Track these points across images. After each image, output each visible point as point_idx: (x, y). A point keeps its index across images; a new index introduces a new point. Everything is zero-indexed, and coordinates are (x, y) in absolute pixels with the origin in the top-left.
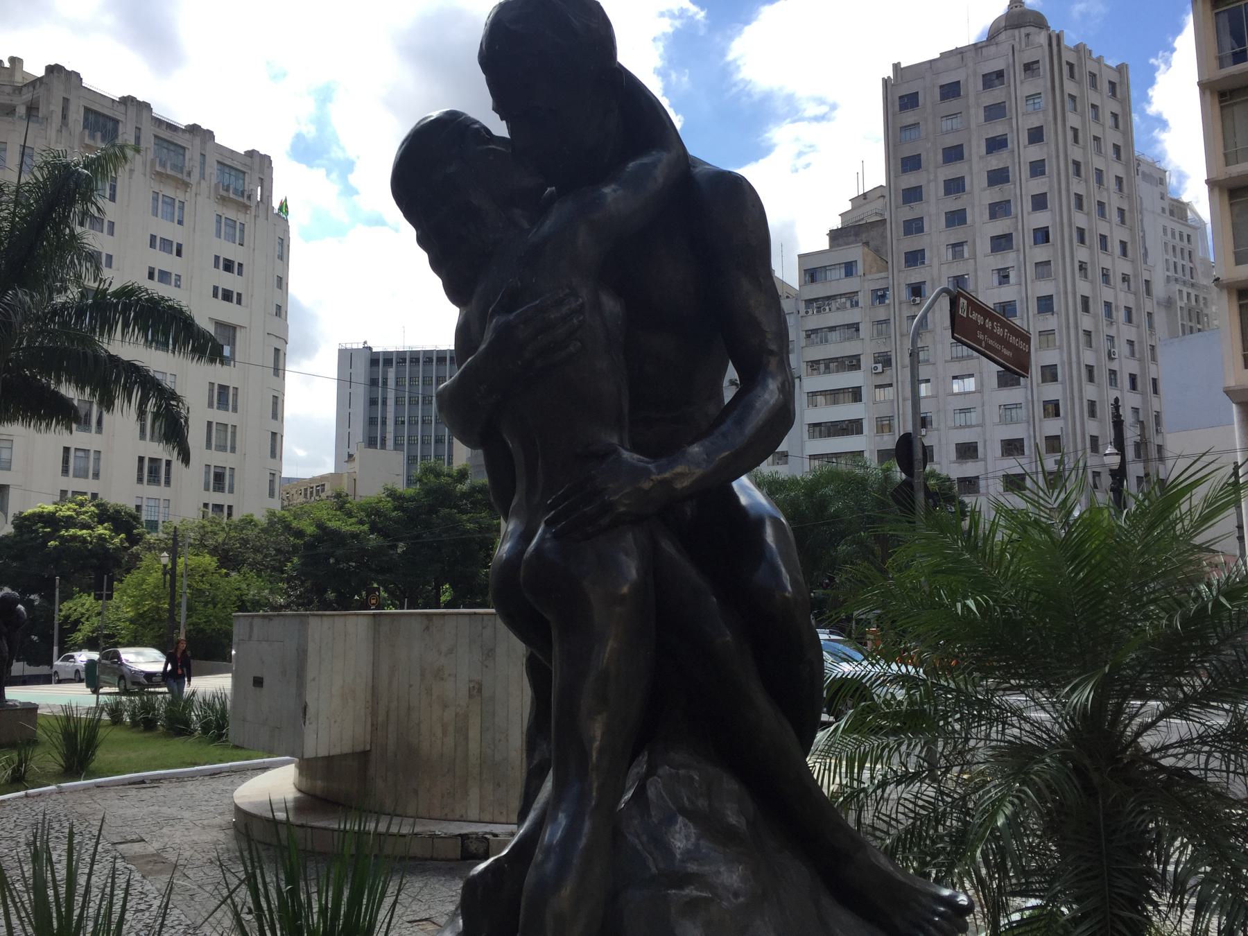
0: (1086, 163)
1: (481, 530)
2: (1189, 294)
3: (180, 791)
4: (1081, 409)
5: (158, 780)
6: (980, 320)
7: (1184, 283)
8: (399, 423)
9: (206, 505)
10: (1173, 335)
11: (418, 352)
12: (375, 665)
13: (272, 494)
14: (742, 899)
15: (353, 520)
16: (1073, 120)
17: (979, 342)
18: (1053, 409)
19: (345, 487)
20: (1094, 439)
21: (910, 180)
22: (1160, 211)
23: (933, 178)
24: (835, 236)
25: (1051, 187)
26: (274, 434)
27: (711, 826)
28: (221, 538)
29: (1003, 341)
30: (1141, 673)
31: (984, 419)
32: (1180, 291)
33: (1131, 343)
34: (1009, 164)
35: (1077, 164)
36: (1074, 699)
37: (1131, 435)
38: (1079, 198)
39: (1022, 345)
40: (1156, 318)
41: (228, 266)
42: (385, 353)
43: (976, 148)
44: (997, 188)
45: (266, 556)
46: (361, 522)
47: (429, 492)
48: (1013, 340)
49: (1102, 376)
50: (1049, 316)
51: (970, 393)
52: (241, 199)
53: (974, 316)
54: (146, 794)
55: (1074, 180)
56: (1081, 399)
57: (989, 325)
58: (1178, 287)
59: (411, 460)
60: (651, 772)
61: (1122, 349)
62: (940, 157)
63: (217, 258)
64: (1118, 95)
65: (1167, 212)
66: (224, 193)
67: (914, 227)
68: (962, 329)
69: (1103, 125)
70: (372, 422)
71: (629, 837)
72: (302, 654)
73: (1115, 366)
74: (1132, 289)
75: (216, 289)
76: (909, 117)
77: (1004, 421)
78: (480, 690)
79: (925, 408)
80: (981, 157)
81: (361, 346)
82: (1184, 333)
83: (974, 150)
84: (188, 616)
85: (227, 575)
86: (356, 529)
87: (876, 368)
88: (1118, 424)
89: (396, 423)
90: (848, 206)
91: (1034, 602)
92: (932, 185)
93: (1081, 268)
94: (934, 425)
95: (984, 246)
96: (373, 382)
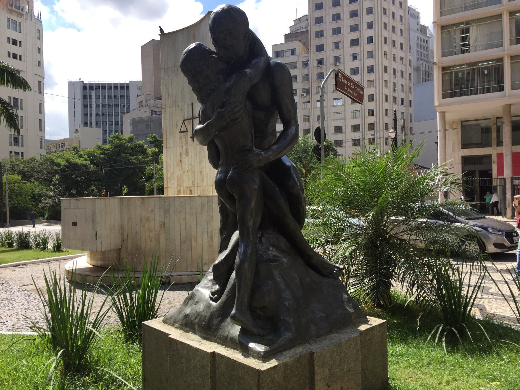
0: (389, 9)
1: (140, 163)
2: (425, 65)
3: (37, 268)
4: (382, 113)
5: (25, 264)
6: (346, 83)
7: (424, 60)
8: (98, 115)
9: (11, 152)
10: (419, 82)
11: (105, 84)
13: (41, 147)
15: (82, 159)
18: (372, 113)
19: (76, 145)
20: (387, 125)
21: (319, 14)
22: (416, 30)
24: (288, 37)
25: (375, 19)
26: (40, 120)
27: (277, 247)
28: (21, 167)
29: (353, 90)
32: (422, 64)
33: (402, 86)
35: (385, 10)
37: (400, 123)
38: (385, 24)
39: (361, 92)
40: (412, 75)
41: (14, 42)
44: (353, 18)
45: (43, 175)
46: (86, 160)
47: (116, 147)
48: (358, 90)
50: (371, 74)
51: (340, 105)
52: (19, 11)
53: (344, 80)
54: (24, 269)
55: (384, 16)
56: (383, 108)
57: (349, 84)
58: (422, 62)
59: (104, 132)
61: (399, 88)
63: (9, 38)
66: (11, 8)
67: (320, 34)
70: (85, 115)
72: (94, 213)
73: (396, 95)
75: (9, 53)
77: (354, 118)
78: (164, 225)
80: (347, 5)
81: (78, 80)
84: (9, 201)
85: (25, 183)
86: (85, 163)
87: (303, 95)
88: (395, 120)
89: (96, 115)
90: (293, 24)
92: (327, 16)
95: (347, 43)
96: (85, 97)
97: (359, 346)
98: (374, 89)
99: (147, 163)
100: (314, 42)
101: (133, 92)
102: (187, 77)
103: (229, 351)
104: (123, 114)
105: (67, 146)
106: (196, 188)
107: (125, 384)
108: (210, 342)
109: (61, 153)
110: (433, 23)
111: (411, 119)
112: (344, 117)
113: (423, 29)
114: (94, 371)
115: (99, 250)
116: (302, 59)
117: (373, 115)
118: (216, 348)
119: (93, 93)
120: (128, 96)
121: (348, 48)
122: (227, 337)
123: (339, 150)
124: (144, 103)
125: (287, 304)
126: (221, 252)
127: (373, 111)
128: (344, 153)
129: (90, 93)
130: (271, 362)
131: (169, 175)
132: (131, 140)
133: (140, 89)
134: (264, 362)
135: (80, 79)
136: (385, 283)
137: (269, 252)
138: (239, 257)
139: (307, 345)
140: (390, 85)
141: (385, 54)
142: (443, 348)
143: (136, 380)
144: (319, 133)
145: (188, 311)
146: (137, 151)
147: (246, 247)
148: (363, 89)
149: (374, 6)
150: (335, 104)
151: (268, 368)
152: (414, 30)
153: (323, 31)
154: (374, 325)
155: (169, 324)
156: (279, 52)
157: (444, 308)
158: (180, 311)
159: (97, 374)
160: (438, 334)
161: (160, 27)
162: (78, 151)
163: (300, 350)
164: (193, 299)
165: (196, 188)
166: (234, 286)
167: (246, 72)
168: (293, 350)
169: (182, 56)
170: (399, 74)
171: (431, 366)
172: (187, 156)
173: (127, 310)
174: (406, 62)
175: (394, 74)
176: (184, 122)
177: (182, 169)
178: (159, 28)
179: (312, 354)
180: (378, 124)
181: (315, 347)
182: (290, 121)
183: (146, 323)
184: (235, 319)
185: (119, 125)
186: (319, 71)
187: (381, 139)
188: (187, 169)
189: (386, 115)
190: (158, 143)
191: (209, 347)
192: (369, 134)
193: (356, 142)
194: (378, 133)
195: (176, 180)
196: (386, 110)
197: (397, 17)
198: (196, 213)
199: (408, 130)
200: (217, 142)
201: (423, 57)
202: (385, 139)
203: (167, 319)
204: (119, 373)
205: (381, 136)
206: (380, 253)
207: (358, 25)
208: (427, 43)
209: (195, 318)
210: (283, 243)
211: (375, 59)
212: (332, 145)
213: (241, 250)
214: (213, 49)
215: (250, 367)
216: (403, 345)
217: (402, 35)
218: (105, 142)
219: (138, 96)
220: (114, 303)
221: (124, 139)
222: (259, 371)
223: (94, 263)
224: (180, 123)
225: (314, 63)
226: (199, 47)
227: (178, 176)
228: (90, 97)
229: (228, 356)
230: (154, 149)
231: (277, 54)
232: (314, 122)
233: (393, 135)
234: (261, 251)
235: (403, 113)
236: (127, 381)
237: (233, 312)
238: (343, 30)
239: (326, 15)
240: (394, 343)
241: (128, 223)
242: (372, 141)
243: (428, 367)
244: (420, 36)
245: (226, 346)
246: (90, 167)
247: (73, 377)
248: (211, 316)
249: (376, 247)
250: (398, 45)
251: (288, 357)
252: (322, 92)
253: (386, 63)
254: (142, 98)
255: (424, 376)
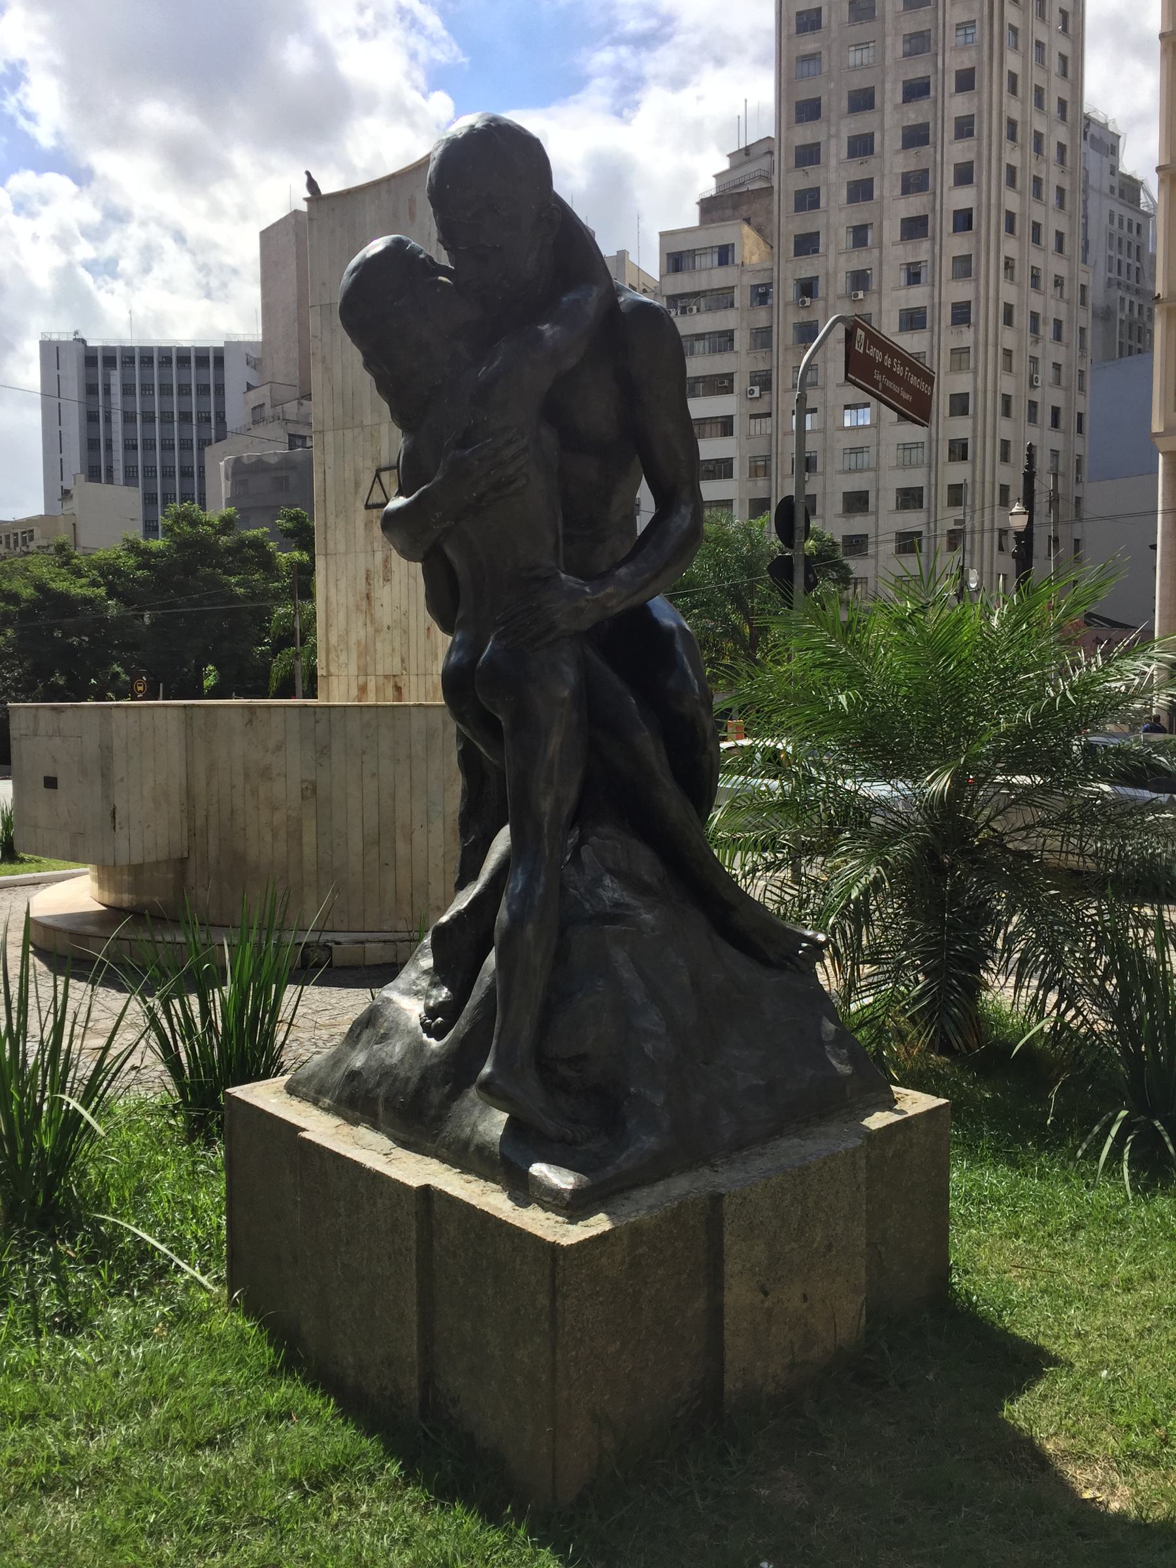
0: (1024, 123)
1: (253, 597)
2: (1131, 303)
4: (992, 451)
6: (879, 359)
12: (189, 764)
14: (657, 933)
15: (84, 581)
16: (1013, 62)
17: (875, 384)
18: (959, 451)
19: (64, 537)
20: (1005, 489)
21: (806, 134)
22: (1107, 190)
23: (835, 132)
24: (709, 207)
25: (979, 154)
29: (900, 381)
30: (995, 763)
31: (878, 463)
32: (1122, 299)
33: (1057, 366)
34: (930, 119)
35: (1012, 124)
36: (934, 786)
37: (1044, 483)
38: (1011, 170)
39: (923, 387)
42: (105, 348)
43: (891, 93)
44: (913, 151)
46: (94, 584)
47: (183, 545)
48: (914, 380)
49: (1019, 408)
50: (964, 328)
51: (864, 427)
53: (873, 351)
55: (1008, 145)
56: (994, 437)
57: (888, 363)
58: (1120, 293)
59: (149, 499)
60: (582, 841)
61: (1046, 373)
62: (845, 104)
64: (1070, 31)
65: (1117, 191)
67: (808, 200)
68: (859, 368)
69: (1048, 71)
70: (92, 445)
71: (571, 890)
72: (106, 751)
73: (1036, 396)
74: (1066, 296)
76: (809, 44)
77: (904, 466)
78: (314, 791)
79: (811, 445)
80: (896, 107)
81: (71, 338)
82: (1121, 355)
83: (888, 95)
86: (89, 592)
87: (752, 392)
88: (1029, 477)
91: (904, 697)
92: (833, 142)
93: (1007, 264)
94: (819, 468)
95: (891, 231)
97: (862, 1177)
98: (971, 376)
99: (277, 597)
100: (793, 225)
101: (235, 376)
102: (359, 346)
103: (473, 1186)
104: (204, 443)
105: (39, 540)
106: (413, 679)
107: (177, 1266)
108: (419, 1157)
109: (19, 563)
110: (1159, 169)
111: (1079, 470)
112: (873, 465)
113: (1130, 188)
114: (90, 1225)
115: (123, 861)
116: (749, 280)
117: (965, 458)
118: (434, 1174)
119: (116, 378)
120: (220, 389)
121: (894, 244)
122: (467, 1143)
123: (857, 566)
124: (268, 411)
125: (648, 1048)
126: (461, 885)
127: (965, 446)
128: (870, 574)
129: (107, 377)
130: (592, 1220)
131: (334, 640)
132: (227, 524)
133: (254, 367)
134: (573, 1220)
135: (76, 333)
136: (962, 981)
137: (601, 891)
138: (509, 908)
139: (706, 1171)
140: (1021, 364)
141: (1009, 264)
142: (1122, 1179)
143: (210, 1255)
144: (790, 517)
145: (358, 1060)
146: (245, 561)
147: (531, 879)
148: (929, 379)
149: (980, 112)
150: (847, 423)
151: (582, 1238)
152: (1100, 192)
153: (818, 189)
154: (910, 1113)
155: (304, 1098)
156: (680, 253)
157: (1134, 1060)
158: (336, 1060)
159: (97, 1233)
160: (1110, 1140)
161: (308, 173)
162: (71, 557)
163: (680, 1186)
164: (374, 1026)
165: (413, 679)
166: (491, 990)
167: (541, 334)
168: (660, 1187)
169: (346, 279)
170: (1047, 331)
171: (1082, 1234)
172: (387, 580)
173: (193, 1048)
174: (1071, 291)
175: (1035, 329)
176: (377, 476)
177: (372, 621)
178: (305, 178)
179: (716, 1199)
180: (978, 486)
181: (725, 1179)
182: (678, 483)
183: (239, 1092)
184: (494, 1094)
185: (192, 480)
186: (804, 316)
187: (987, 535)
188: (387, 621)
189: (1005, 457)
190: (302, 536)
191: (413, 1170)
192: (948, 518)
193: (908, 543)
194: (978, 515)
195: (354, 656)
196: (1005, 444)
197: (1051, 151)
198: (410, 757)
199: (1066, 509)
200: (449, 551)
201: (1123, 278)
202: (996, 534)
203: (298, 1082)
204: (161, 1233)
205: (987, 525)
206: (949, 888)
207: (926, 171)
208: (1138, 232)
209: (379, 1084)
210: (646, 864)
211: (977, 280)
212: (834, 551)
213: (516, 883)
214: (443, 258)
215: (530, 1233)
216: (1003, 1169)
217: (1061, 205)
218: (150, 529)
219: (250, 387)
220: (154, 1023)
221: (208, 524)
222: (554, 1246)
223: (109, 898)
224: (368, 478)
225: (789, 292)
226: (397, 250)
227: (359, 643)
228: (107, 391)
229: (467, 1200)
230: (296, 554)
231: (675, 261)
232: (784, 477)
233: (1019, 522)
234: (576, 888)
235: (1055, 453)
236: (183, 1255)
237: (487, 1069)
238: (882, 187)
239: (829, 137)
240: (977, 1160)
241: (208, 784)
242: (955, 538)
243: (1073, 1235)
244: (1119, 209)
245: (466, 1169)
246: (107, 607)
247: (26, 1243)
248: (423, 1078)
249: (941, 871)
250: (1048, 239)
251: (647, 1205)
252: (807, 381)
253: (1009, 293)
254: (261, 395)
255: (1057, 1265)
